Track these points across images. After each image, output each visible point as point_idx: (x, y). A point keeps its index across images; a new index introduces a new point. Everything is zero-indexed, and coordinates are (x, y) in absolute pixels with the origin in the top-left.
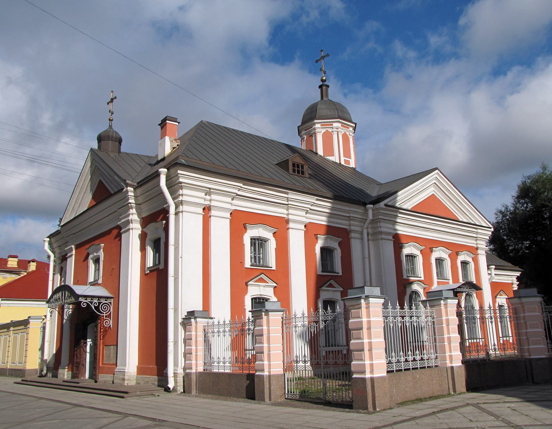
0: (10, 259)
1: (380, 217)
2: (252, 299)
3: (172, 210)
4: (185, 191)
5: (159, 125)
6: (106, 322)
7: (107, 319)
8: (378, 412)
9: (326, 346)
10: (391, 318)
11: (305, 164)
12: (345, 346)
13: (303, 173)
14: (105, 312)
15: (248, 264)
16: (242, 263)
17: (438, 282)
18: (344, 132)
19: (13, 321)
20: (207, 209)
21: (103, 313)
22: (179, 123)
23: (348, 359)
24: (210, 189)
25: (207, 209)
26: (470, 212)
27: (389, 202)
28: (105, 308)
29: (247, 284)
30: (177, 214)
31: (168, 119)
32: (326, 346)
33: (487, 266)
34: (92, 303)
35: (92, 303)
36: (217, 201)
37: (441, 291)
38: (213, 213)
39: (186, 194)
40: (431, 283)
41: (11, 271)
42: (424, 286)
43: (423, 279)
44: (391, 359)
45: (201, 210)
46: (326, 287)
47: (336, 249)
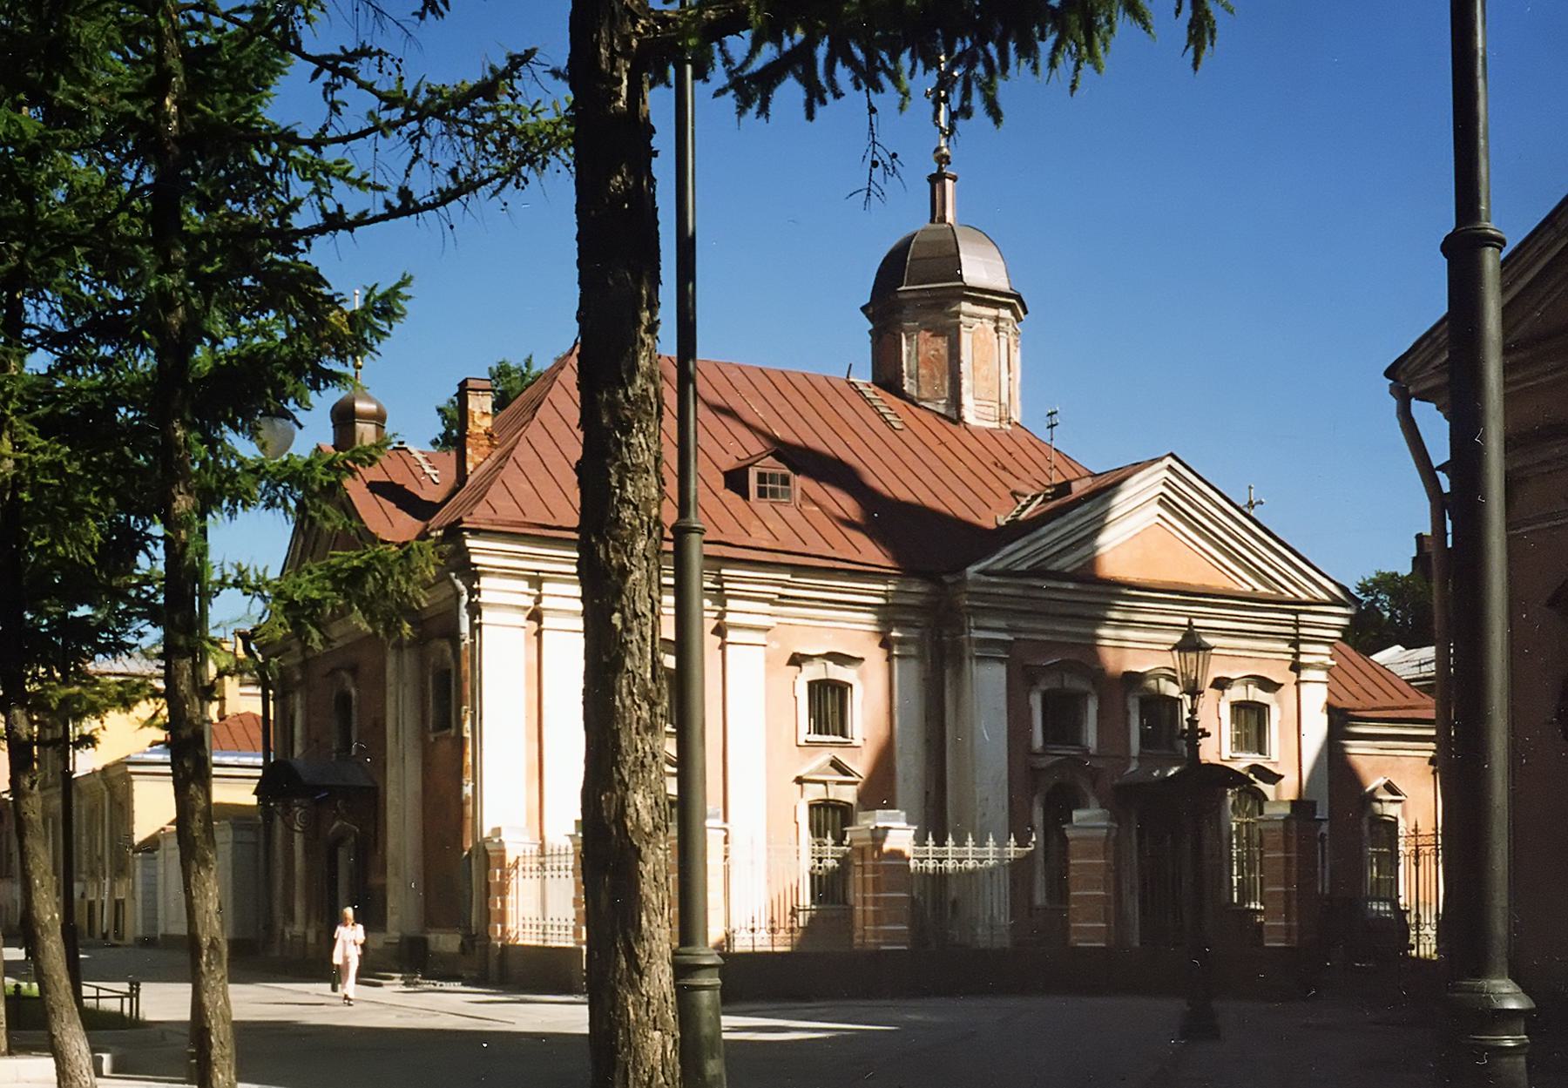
20: (536, 616)
27: (994, 563)
31: (471, 384)
45: (521, 618)
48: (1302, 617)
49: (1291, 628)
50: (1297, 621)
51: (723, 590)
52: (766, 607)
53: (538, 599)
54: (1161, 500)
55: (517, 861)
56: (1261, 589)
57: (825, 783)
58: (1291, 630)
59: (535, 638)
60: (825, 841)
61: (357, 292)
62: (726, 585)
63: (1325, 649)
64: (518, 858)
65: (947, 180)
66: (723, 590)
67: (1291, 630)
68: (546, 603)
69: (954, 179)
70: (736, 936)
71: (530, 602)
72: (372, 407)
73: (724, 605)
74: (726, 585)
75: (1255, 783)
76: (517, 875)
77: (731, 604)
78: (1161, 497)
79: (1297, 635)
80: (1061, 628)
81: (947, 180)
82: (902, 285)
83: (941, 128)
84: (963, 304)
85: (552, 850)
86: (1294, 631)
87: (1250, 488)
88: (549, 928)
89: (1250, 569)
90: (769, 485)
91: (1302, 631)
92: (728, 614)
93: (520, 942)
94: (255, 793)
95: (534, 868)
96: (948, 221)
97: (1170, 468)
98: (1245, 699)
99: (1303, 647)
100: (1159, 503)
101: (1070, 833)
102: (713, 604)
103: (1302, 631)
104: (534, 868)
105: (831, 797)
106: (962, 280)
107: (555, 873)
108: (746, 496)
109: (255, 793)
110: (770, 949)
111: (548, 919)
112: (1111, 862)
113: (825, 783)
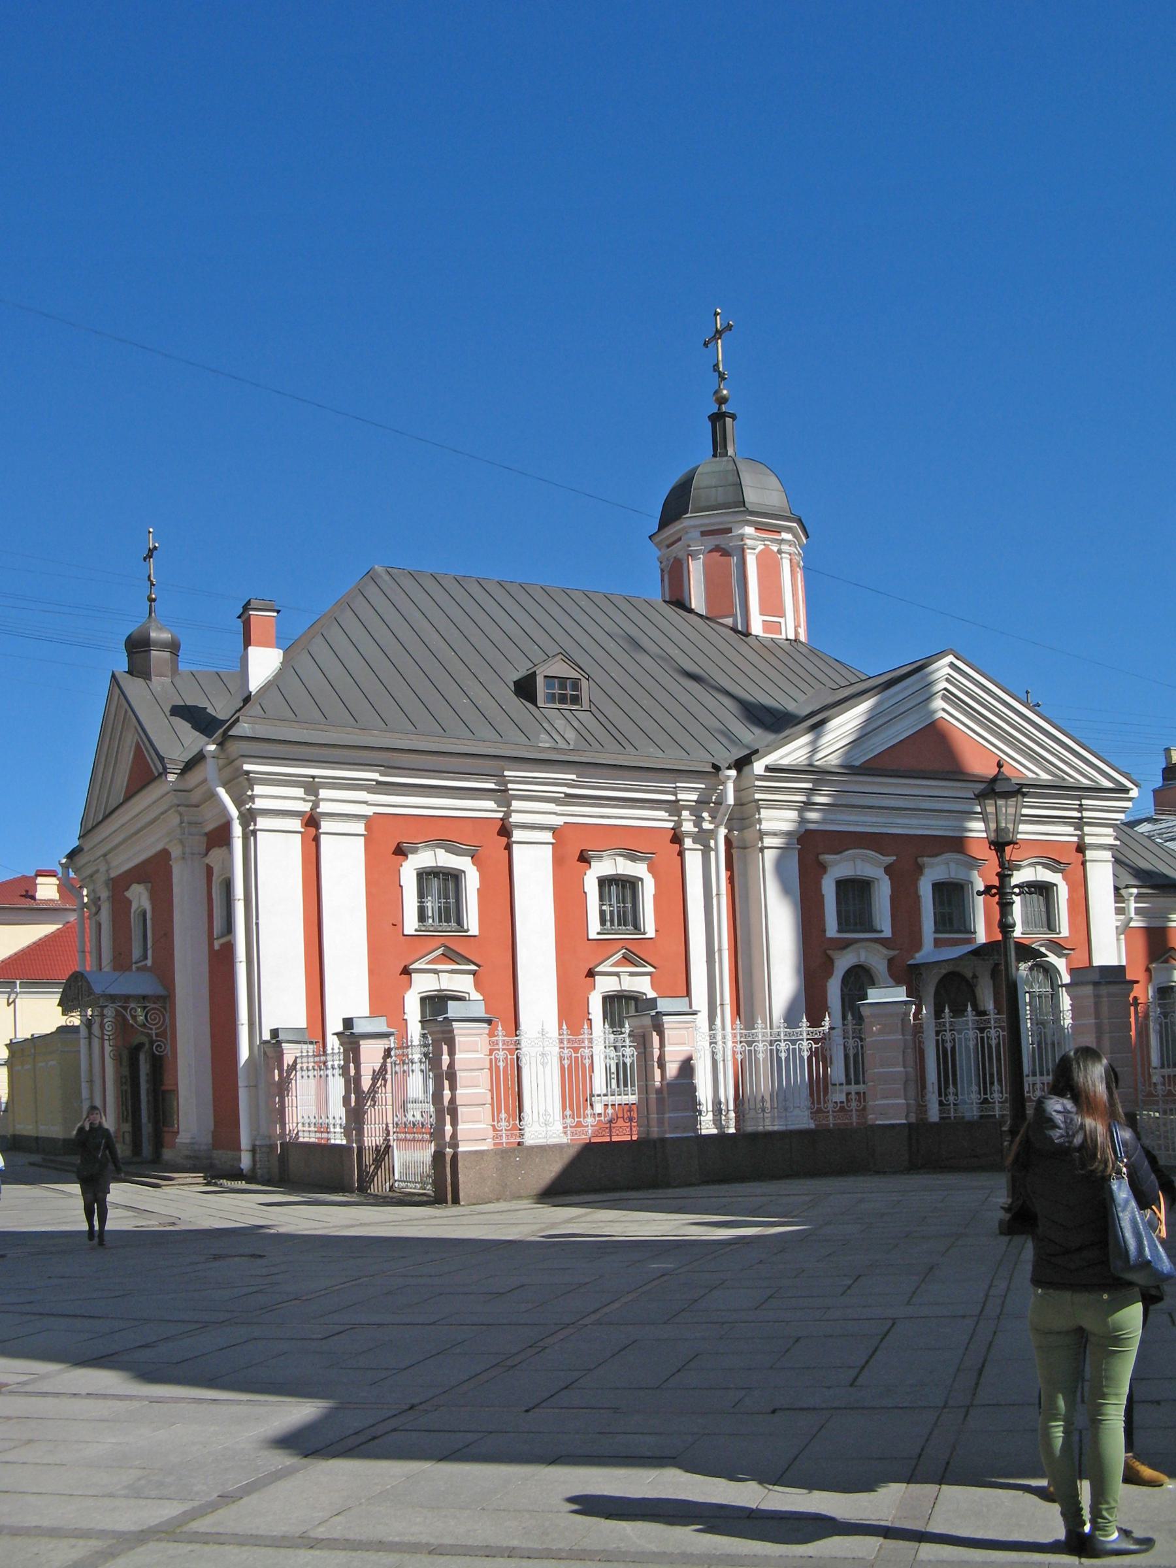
0: (40, 880)
1: (757, 796)
2: (423, 1000)
3: (237, 830)
4: (258, 790)
5: (239, 617)
6: (158, 1046)
7: (159, 1041)
8: (463, 1206)
9: (848, 1082)
10: (501, 1053)
11: (581, 677)
12: (841, 1084)
13: (576, 700)
14: (154, 1027)
15: (411, 924)
16: (398, 924)
17: (936, 939)
18: (763, 547)
19: (35, 1036)
20: (312, 821)
21: (151, 1029)
22: (278, 612)
23: (520, 1120)
24: (313, 777)
25: (312, 821)
26: (906, 795)
27: (781, 758)
28: (152, 1017)
29: (406, 971)
30: (247, 836)
31: (254, 604)
32: (848, 1082)
33: (1117, 889)
34: (125, 1008)
35: (125, 1008)
36: (331, 801)
37: (688, 993)
38: (325, 826)
39: (265, 796)
40: (917, 945)
41: (44, 912)
42: (884, 951)
43: (887, 933)
44: (582, 1119)
45: (296, 824)
46: (612, 966)
47: (641, 880)
48: (1084, 802)
49: (1076, 812)
50: (1081, 805)
51: (507, 790)
52: (551, 807)
53: (316, 805)
54: (944, 694)
55: (295, 1062)
56: (1045, 776)
57: (617, 974)
58: (1076, 814)
59: (314, 843)
60: (623, 1030)
61: (151, 530)
62: (510, 786)
63: (1110, 831)
64: (296, 1058)
65: (727, 419)
66: (507, 790)
67: (1076, 814)
68: (324, 807)
69: (733, 417)
70: (702, 1118)
71: (306, 807)
72: (166, 636)
73: (509, 805)
74: (510, 786)
75: (1047, 956)
76: (296, 1074)
77: (516, 804)
78: (944, 692)
79: (1081, 818)
80: (852, 818)
81: (727, 419)
82: (687, 513)
83: (719, 372)
84: (746, 528)
85: (333, 1049)
86: (1079, 815)
87: (1027, 692)
88: (331, 1126)
89: (1030, 755)
90: (947, 1020)
91: (1086, 814)
92: (513, 814)
93: (301, 1140)
94: (59, 1005)
95: (310, 1068)
96: (729, 454)
97: (952, 665)
98: (1034, 879)
99: (1087, 829)
100: (942, 699)
101: (865, 1012)
102: (498, 807)
103: (1086, 814)
104: (310, 1068)
105: (625, 987)
106: (744, 506)
107: (305, 1073)
108: (534, 702)
109: (59, 1005)
110: (607, 1139)
111: (331, 1117)
112: (909, 1037)
113: (617, 974)
